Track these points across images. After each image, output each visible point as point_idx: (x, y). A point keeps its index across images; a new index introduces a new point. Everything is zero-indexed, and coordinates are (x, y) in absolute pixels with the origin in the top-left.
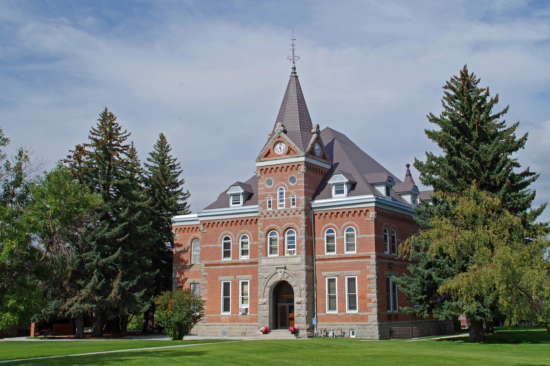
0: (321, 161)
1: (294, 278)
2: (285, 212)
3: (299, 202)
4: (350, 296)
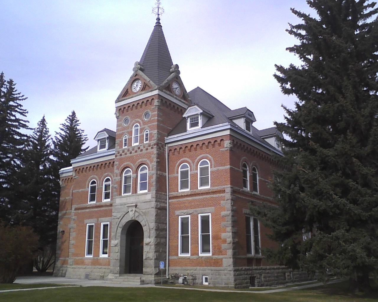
0: (180, 101)
1: (144, 216)
2: (139, 148)
3: (152, 136)
4: (203, 236)
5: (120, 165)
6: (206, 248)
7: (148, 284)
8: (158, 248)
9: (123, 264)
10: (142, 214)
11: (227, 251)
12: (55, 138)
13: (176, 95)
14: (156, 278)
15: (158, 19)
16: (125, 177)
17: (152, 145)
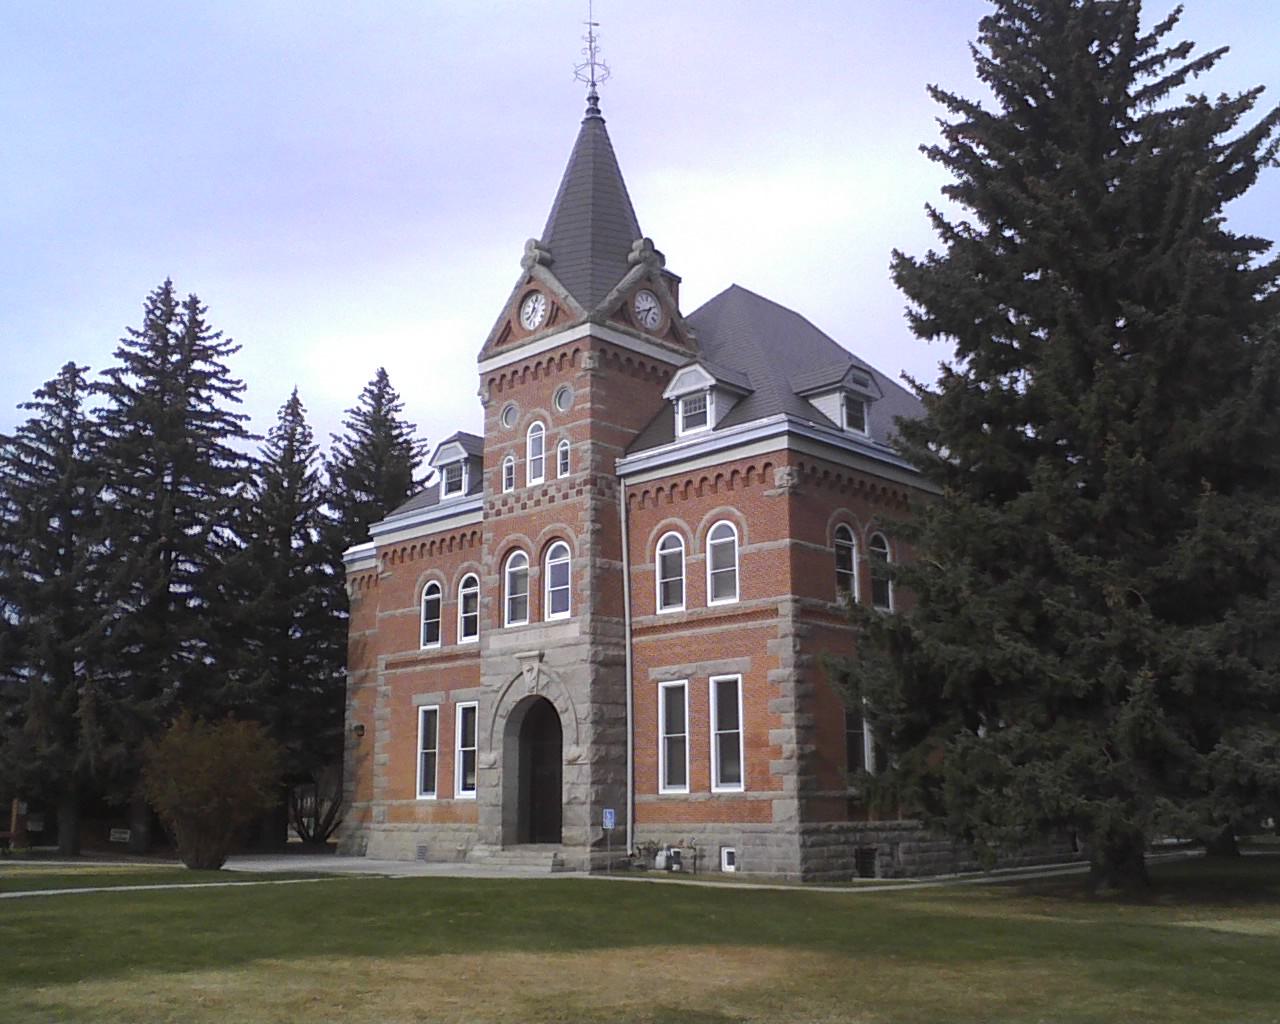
2: (545, 493)
5: (496, 542)
6: (730, 770)
7: (574, 870)
8: (602, 771)
9: (514, 817)
10: (558, 680)
11: (785, 777)
12: (331, 452)
13: (647, 331)
14: (597, 855)
15: (594, 99)
16: (513, 575)
17: (579, 485)
